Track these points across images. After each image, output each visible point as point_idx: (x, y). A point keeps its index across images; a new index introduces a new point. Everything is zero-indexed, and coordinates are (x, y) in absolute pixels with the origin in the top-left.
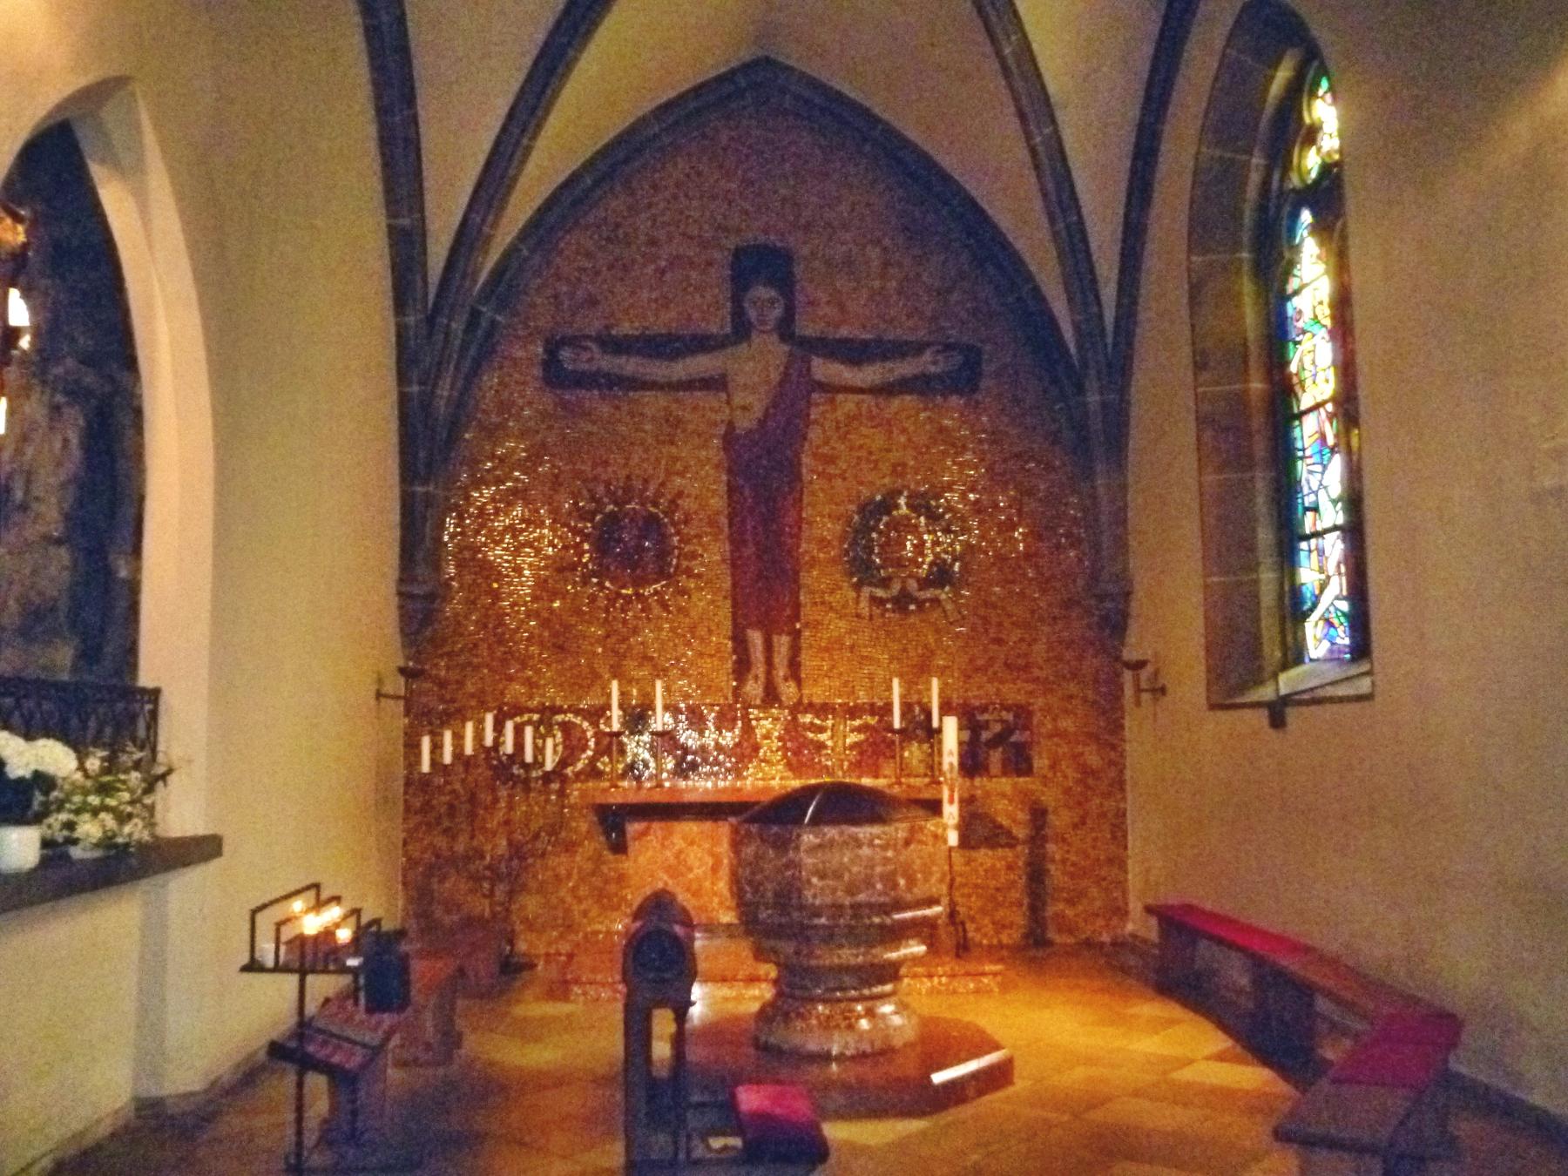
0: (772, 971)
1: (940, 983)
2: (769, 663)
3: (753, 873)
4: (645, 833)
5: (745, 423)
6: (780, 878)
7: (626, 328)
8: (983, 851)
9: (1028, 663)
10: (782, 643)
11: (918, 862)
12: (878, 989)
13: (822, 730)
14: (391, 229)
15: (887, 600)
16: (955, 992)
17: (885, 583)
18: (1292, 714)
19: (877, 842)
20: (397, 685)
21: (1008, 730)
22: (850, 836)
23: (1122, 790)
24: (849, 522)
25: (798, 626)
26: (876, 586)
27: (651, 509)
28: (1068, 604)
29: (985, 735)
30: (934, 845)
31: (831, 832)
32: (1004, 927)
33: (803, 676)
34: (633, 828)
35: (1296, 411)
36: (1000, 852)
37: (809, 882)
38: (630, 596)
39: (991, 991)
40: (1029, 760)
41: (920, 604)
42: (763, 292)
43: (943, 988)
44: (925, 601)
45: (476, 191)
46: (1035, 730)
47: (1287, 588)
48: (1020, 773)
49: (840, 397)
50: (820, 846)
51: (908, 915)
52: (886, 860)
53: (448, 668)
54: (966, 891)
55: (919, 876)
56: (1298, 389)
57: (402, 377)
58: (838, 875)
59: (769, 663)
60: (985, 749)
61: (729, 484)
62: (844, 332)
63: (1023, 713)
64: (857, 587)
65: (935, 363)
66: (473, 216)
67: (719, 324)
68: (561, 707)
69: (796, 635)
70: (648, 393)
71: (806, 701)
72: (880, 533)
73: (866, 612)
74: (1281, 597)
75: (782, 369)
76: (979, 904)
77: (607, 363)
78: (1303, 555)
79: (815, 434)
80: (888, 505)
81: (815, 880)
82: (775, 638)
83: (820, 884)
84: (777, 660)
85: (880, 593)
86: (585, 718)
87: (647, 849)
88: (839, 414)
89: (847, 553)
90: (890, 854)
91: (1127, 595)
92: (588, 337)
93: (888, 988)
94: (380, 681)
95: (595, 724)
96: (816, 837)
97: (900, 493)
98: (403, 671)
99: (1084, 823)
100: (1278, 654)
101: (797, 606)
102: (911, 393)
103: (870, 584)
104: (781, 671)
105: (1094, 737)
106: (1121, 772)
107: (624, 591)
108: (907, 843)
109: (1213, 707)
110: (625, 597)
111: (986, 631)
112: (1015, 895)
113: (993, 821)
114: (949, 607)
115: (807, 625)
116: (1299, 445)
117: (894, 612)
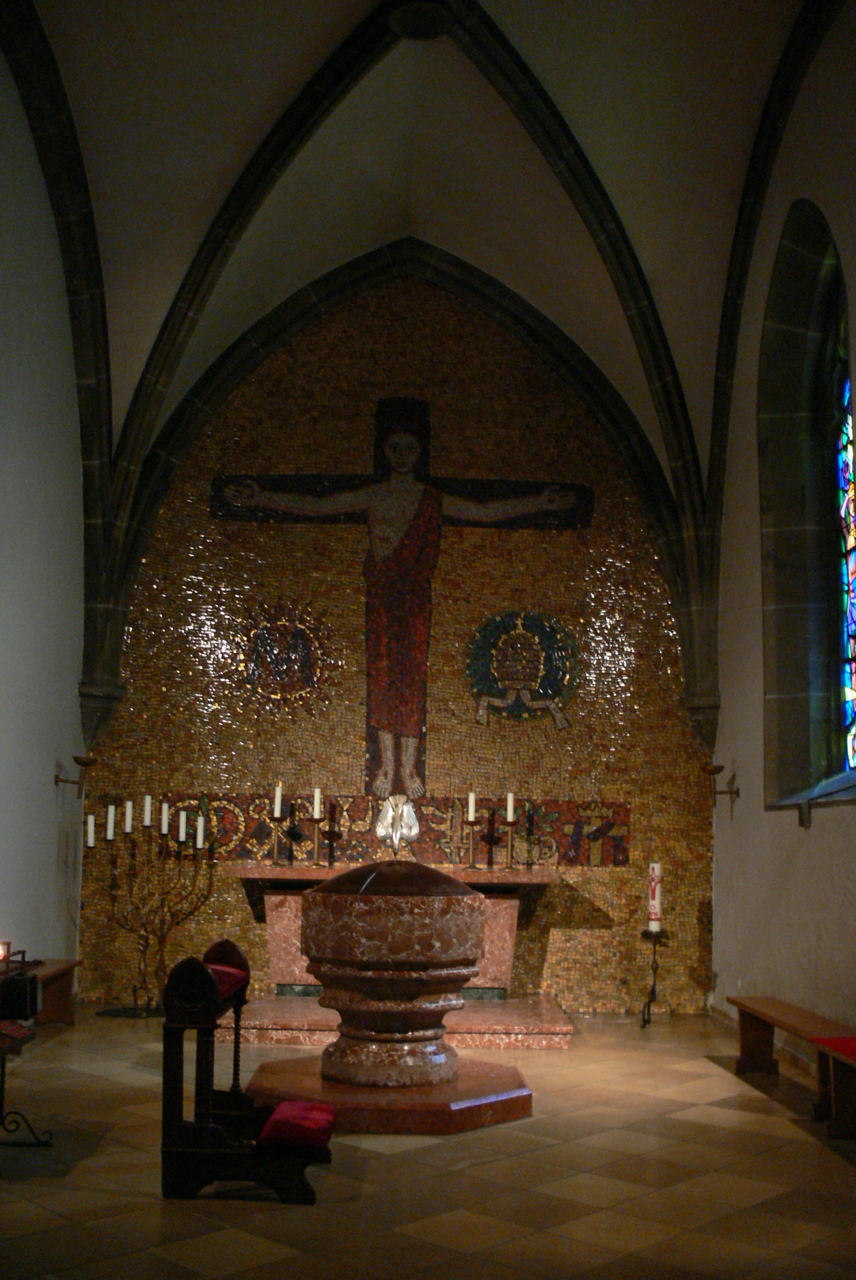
0: (334, 1017)
1: (516, 1040)
2: (398, 763)
3: (317, 933)
4: (281, 904)
5: (383, 551)
6: (337, 937)
7: (285, 469)
8: (581, 931)
9: (627, 767)
10: (410, 744)
11: (454, 929)
12: (420, 1034)
13: (442, 821)
14: (81, 389)
15: (504, 709)
16: (528, 1047)
17: (502, 695)
18: (816, 813)
19: (416, 910)
20: (73, 771)
21: (608, 826)
22: (395, 905)
23: (708, 881)
24: (473, 640)
25: (424, 730)
26: (493, 696)
27: (299, 626)
28: (666, 713)
29: (587, 829)
30: (470, 916)
31: (379, 901)
32: (599, 997)
33: (427, 773)
34: (271, 900)
35: (844, 551)
36: (597, 932)
37: (359, 942)
38: (279, 701)
39: (561, 1048)
40: (625, 851)
41: (532, 712)
42: (405, 439)
43: (520, 1044)
44: (536, 710)
45: (151, 358)
46: (632, 827)
47: (833, 704)
48: (616, 863)
49: (467, 530)
50: (369, 913)
51: (445, 972)
52: (424, 926)
53: (123, 759)
54: (566, 965)
55: (454, 940)
56: (845, 531)
57: (88, 512)
58: (382, 936)
59: (398, 763)
60: (587, 841)
61: (367, 604)
62: (472, 474)
63: (621, 812)
64: (478, 696)
65: (551, 501)
66: (149, 376)
67: (365, 467)
68: (217, 795)
69: (422, 737)
70: (300, 525)
71: (428, 795)
72: (499, 650)
73: (484, 720)
74: (828, 710)
75: (416, 505)
76: (577, 977)
77: (264, 499)
78: (847, 676)
79: (443, 562)
80: (506, 626)
81: (363, 940)
82: (404, 740)
83: (368, 943)
84: (404, 759)
85: (497, 702)
86: (236, 805)
87: (282, 918)
88: (466, 545)
89: (469, 666)
90: (427, 921)
91: (716, 707)
92: (251, 477)
93: (430, 1033)
94: (59, 766)
95: (246, 812)
96: (366, 905)
97: (517, 615)
98: (77, 760)
99: (673, 909)
100: (824, 763)
101: (424, 711)
102: (528, 528)
103: (489, 694)
104: (408, 768)
105: (685, 834)
106: (708, 865)
107: (273, 696)
108: (444, 912)
109: (769, 808)
110: (274, 702)
111: (591, 737)
112: (610, 969)
113: (591, 904)
114: (559, 716)
115: (432, 728)
116: (845, 580)
117: (509, 719)
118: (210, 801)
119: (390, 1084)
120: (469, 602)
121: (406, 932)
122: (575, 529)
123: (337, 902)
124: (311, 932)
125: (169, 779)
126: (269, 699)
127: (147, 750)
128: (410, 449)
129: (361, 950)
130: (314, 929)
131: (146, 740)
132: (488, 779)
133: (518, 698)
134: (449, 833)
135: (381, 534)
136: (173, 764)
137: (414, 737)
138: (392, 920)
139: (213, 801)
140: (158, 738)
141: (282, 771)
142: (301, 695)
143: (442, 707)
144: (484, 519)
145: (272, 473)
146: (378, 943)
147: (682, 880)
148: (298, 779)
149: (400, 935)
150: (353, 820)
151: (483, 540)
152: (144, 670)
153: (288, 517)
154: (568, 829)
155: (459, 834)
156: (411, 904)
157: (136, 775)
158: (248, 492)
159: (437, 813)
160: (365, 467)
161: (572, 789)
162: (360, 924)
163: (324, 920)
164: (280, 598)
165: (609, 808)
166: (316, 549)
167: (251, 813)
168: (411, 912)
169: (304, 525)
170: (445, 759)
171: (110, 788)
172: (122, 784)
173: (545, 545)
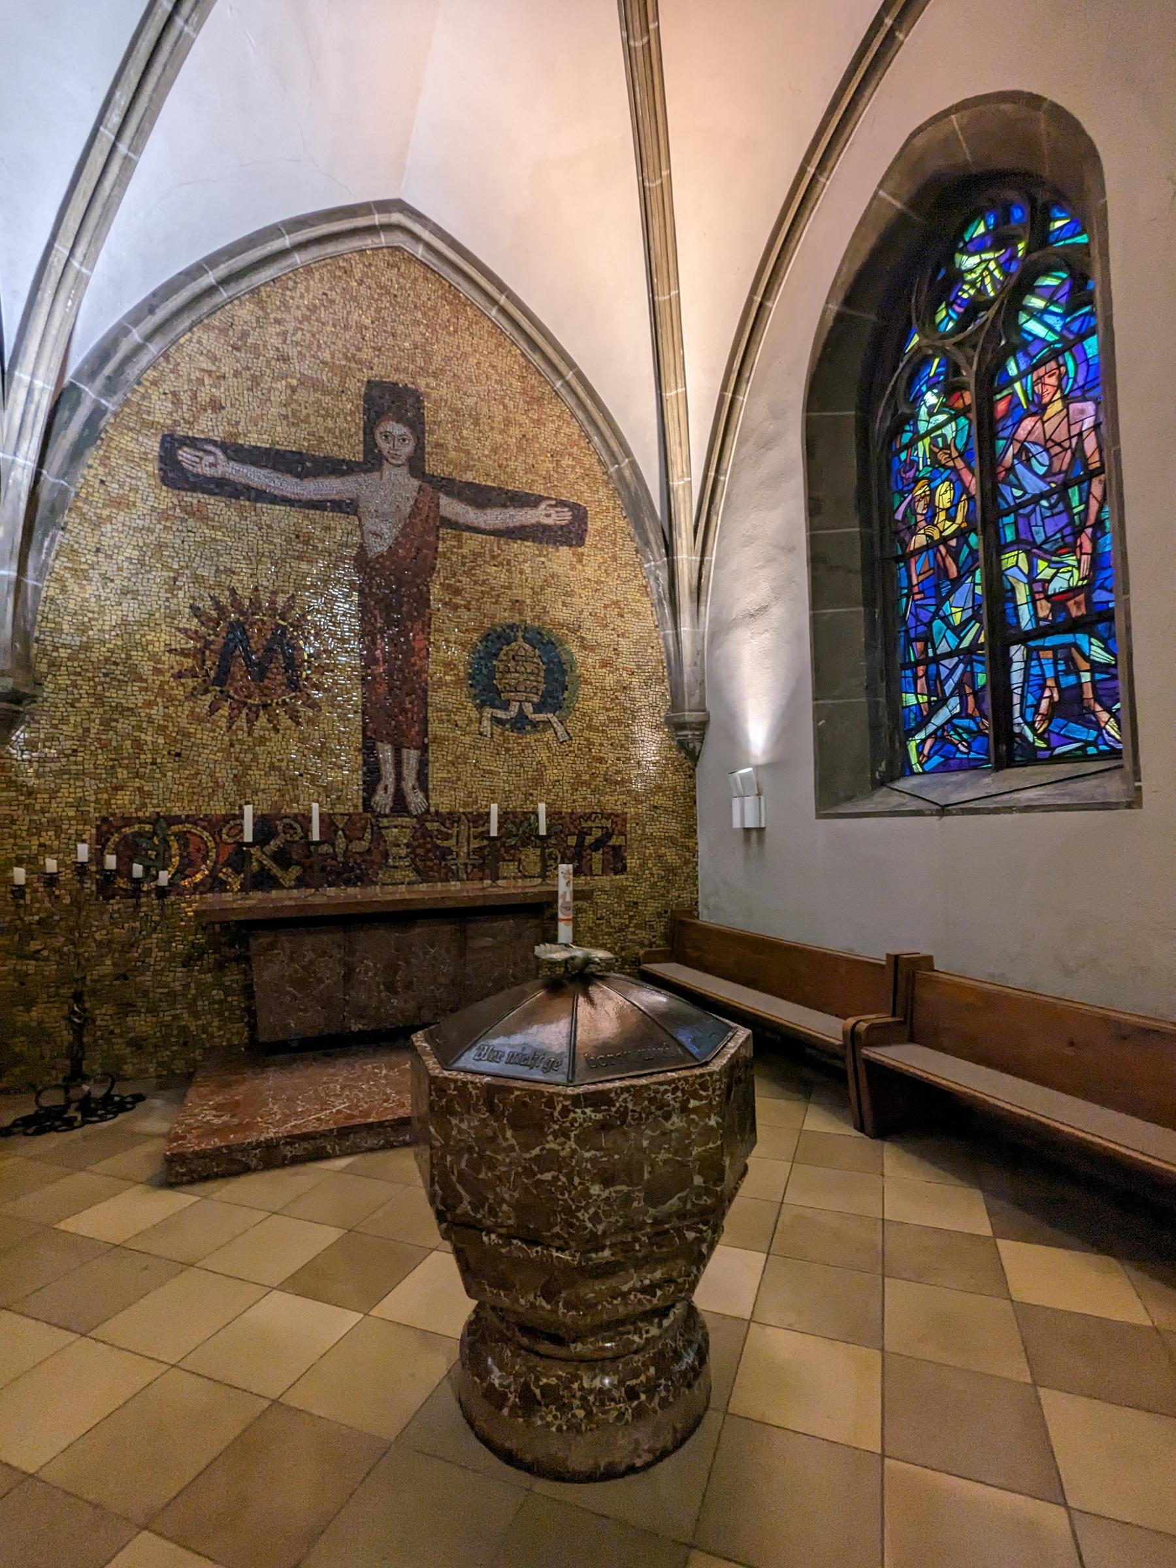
2: (399, 777)
3: (475, 1166)
4: (272, 946)
13: (447, 837)
15: (507, 721)
17: (506, 706)
19: (693, 1103)
33: (430, 786)
41: (534, 725)
42: (398, 429)
49: (466, 534)
50: (604, 1126)
58: (631, 1173)
59: (399, 777)
62: (469, 477)
67: (352, 451)
69: (424, 748)
71: (432, 809)
75: (412, 502)
82: (405, 751)
84: (405, 772)
85: (501, 714)
88: (465, 551)
92: (214, 443)
103: (493, 706)
104: (410, 782)
114: (560, 729)
118: (170, 825)
119: (639, 1463)
120: (469, 610)
121: (676, 1153)
122: (571, 546)
123: (524, 1103)
124: (457, 1161)
125: (110, 799)
126: (245, 704)
127: (76, 763)
128: (404, 440)
129: (592, 1210)
130: (466, 1156)
131: (75, 751)
132: (493, 792)
133: (521, 710)
134: (454, 849)
135: (374, 528)
136: (115, 780)
137: (415, 748)
138: (648, 1132)
139: (173, 824)
140: (93, 748)
141: (262, 787)
142: (284, 701)
143: (445, 718)
144: (483, 525)
145: (241, 442)
146: (625, 1188)
147: (673, 885)
148: (283, 796)
149: (665, 1162)
150: (349, 839)
151: (482, 547)
152: (69, 664)
153: (260, 495)
154: (572, 841)
155: (465, 849)
156: (683, 1090)
157: (60, 795)
158: (211, 459)
159: (442, 828)
160: (352, 451)
161: (574, 801)
162: (587, 1155)
163: (493, 1139)
164: (256, 589)
165: (607, 819)
166: (297, 537)
167: (224, 837)
168: (684, 1109)
169: (283, 508)
170: (449, 772)
171: (20, 812)
172: (38, 807)
173: (543, 559)
